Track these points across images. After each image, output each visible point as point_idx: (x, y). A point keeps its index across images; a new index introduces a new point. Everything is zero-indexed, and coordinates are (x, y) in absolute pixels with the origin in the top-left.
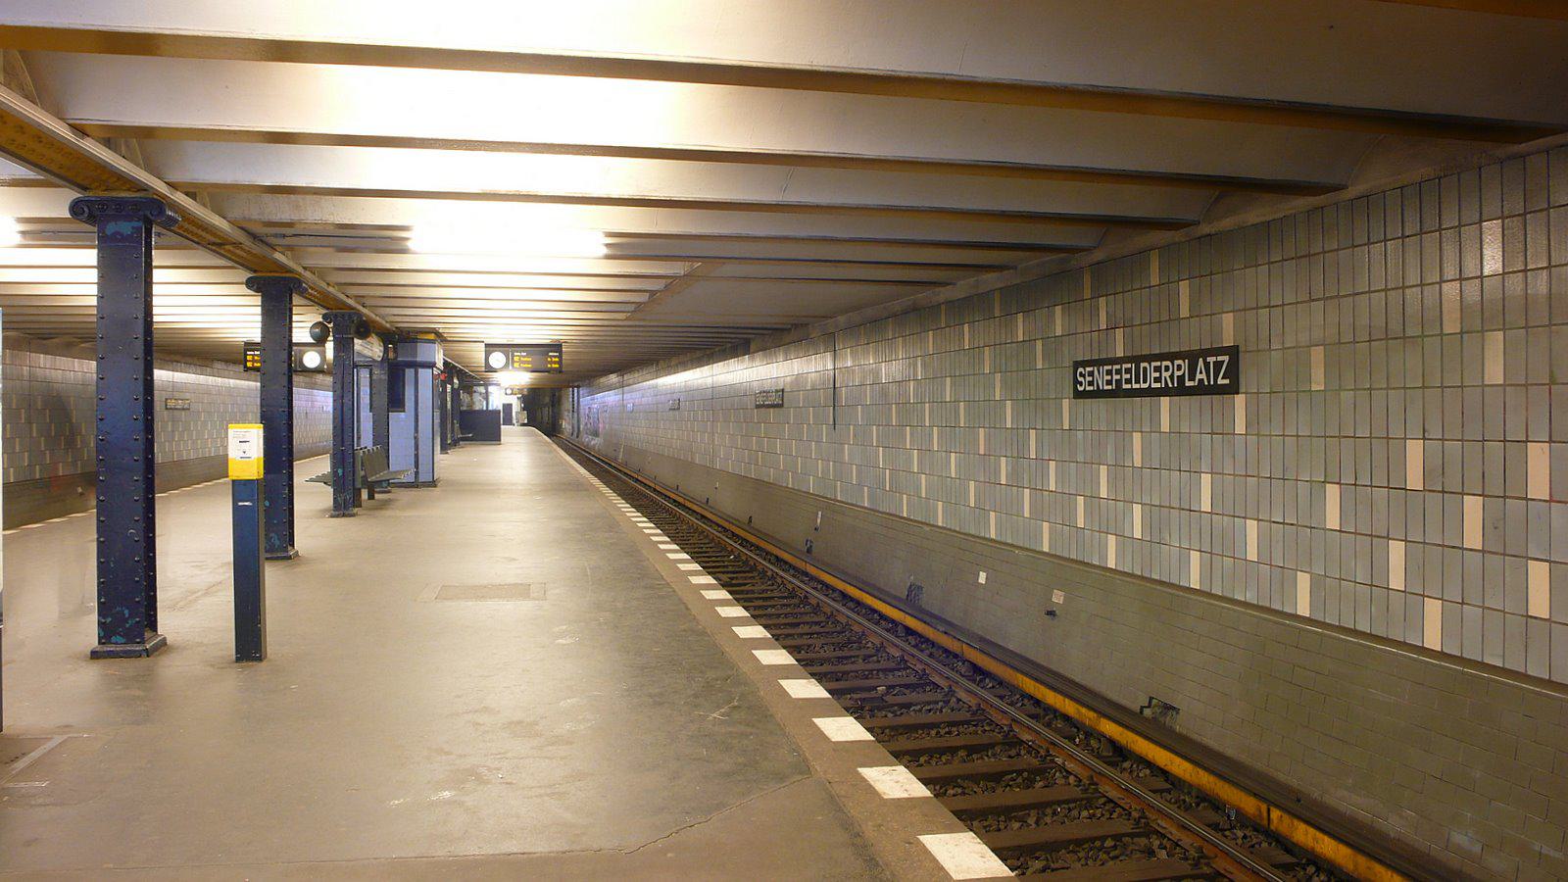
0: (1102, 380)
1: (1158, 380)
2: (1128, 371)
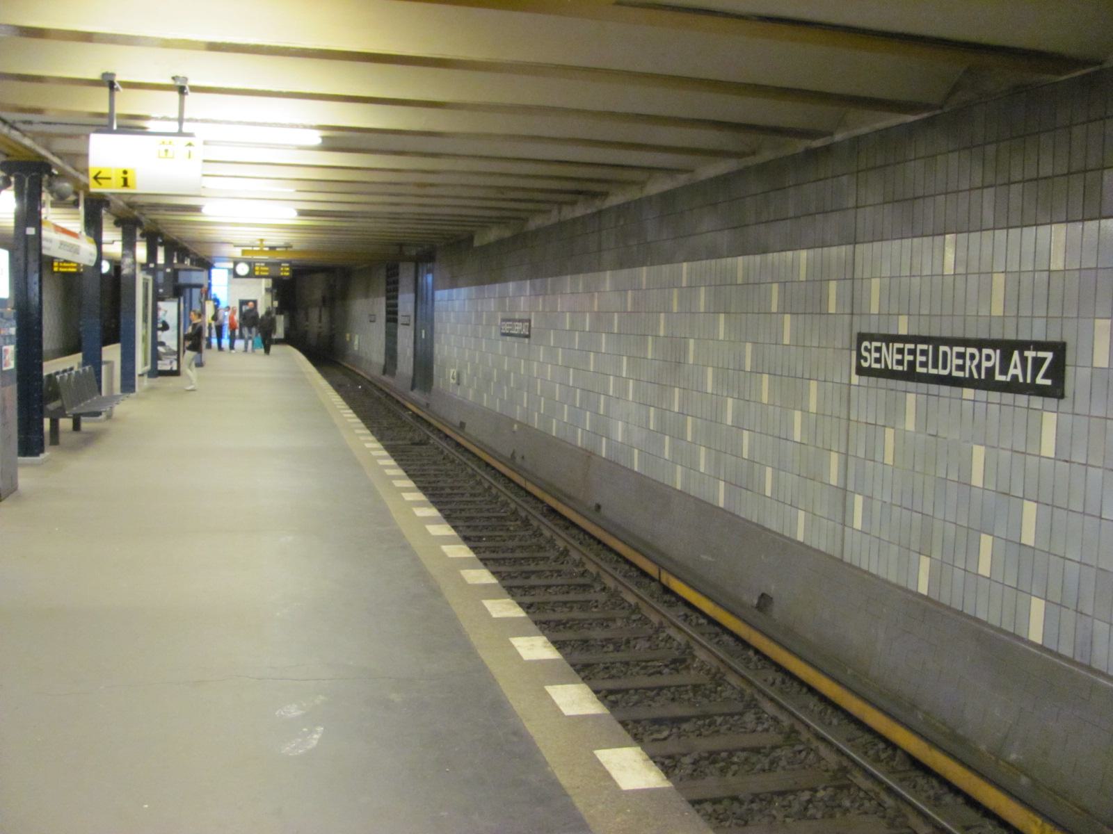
0: (890, 358)
1: (961, 368)
2: (924, 353)
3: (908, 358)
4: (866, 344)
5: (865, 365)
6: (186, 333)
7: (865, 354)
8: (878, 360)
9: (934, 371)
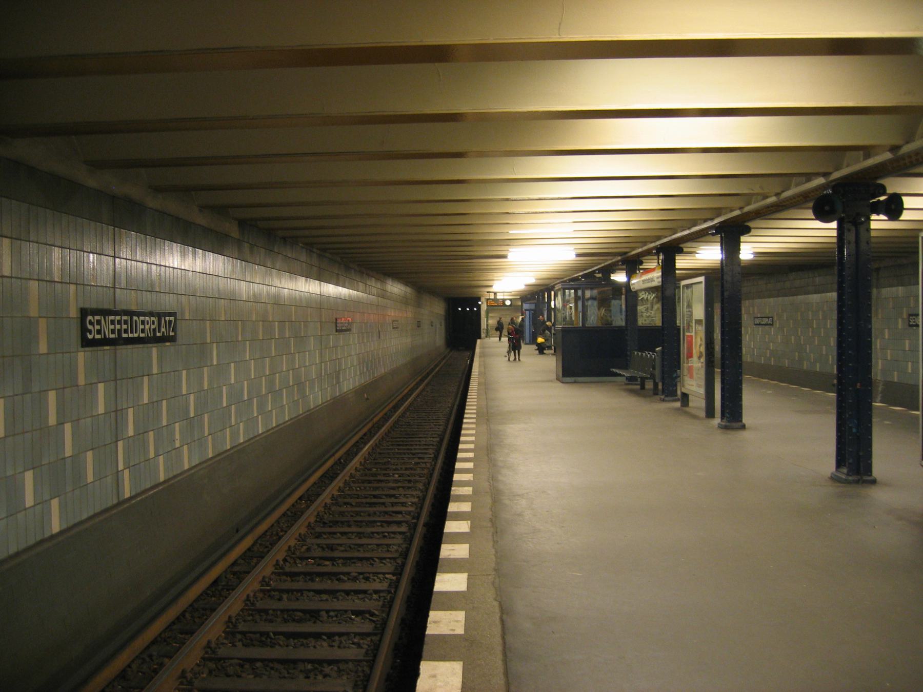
1: (143, 331)
2: (126, 322)
3: (118, 327)
4: (90, 318)
5: (90, 337)
6: (904, 198)
7: (90, 327)
8: (99, 332)
9: (131, 335)
